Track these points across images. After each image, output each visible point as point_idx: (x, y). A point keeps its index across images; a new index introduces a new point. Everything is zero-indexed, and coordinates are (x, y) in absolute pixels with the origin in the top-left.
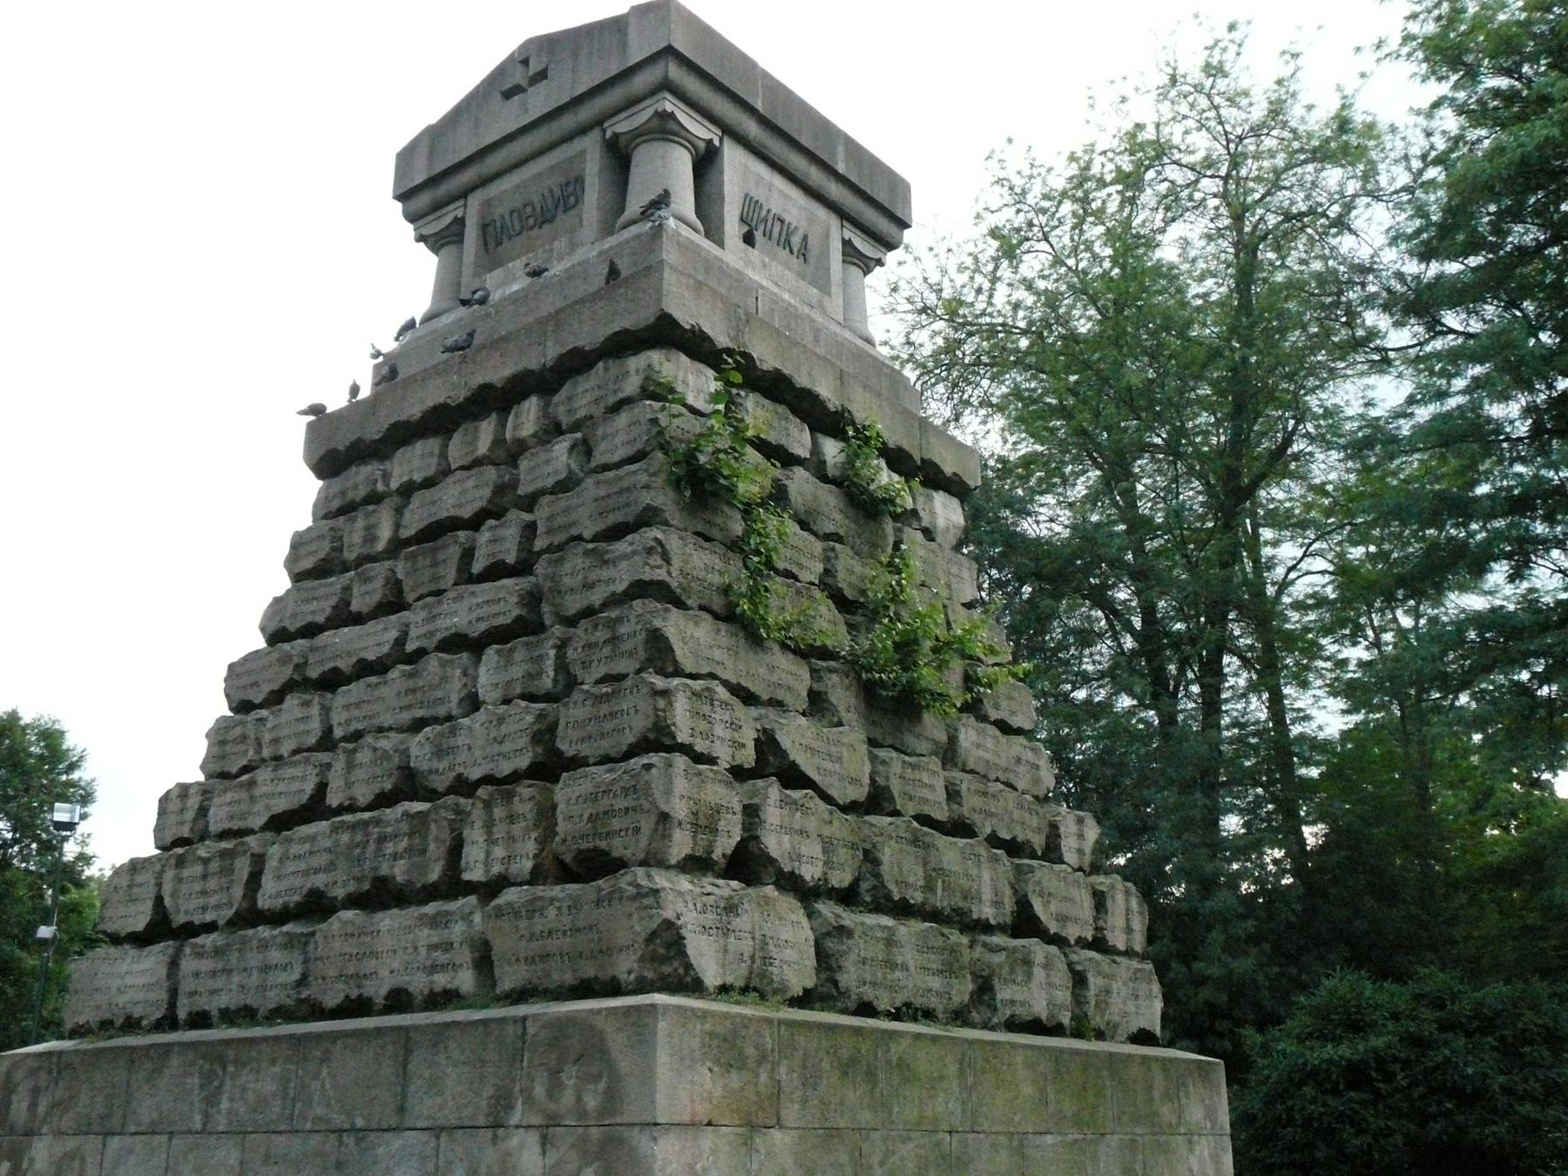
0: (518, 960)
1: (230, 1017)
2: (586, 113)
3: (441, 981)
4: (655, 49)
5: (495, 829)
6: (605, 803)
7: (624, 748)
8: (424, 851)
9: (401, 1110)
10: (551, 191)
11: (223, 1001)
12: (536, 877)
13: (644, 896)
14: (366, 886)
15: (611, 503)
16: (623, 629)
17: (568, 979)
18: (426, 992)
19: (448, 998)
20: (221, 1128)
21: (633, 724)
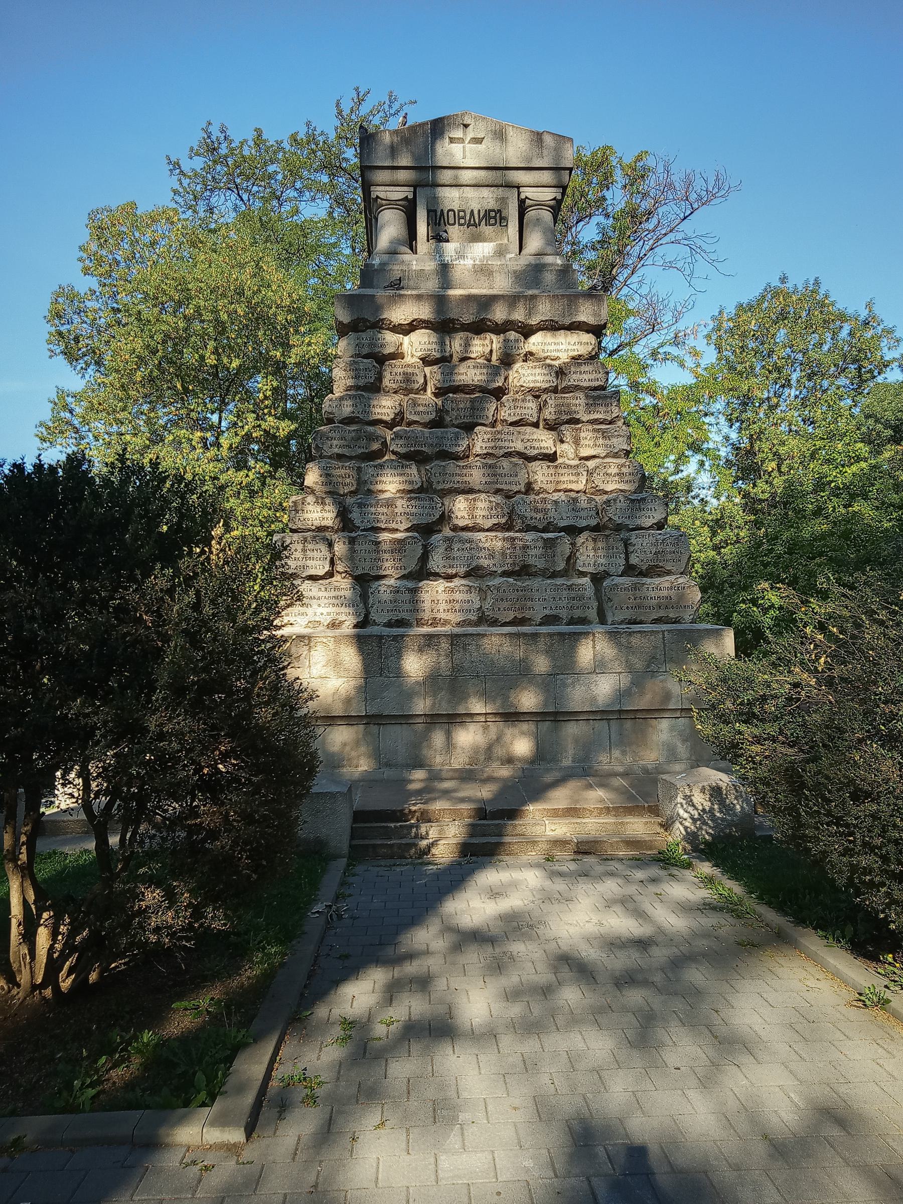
3: (577, 613)
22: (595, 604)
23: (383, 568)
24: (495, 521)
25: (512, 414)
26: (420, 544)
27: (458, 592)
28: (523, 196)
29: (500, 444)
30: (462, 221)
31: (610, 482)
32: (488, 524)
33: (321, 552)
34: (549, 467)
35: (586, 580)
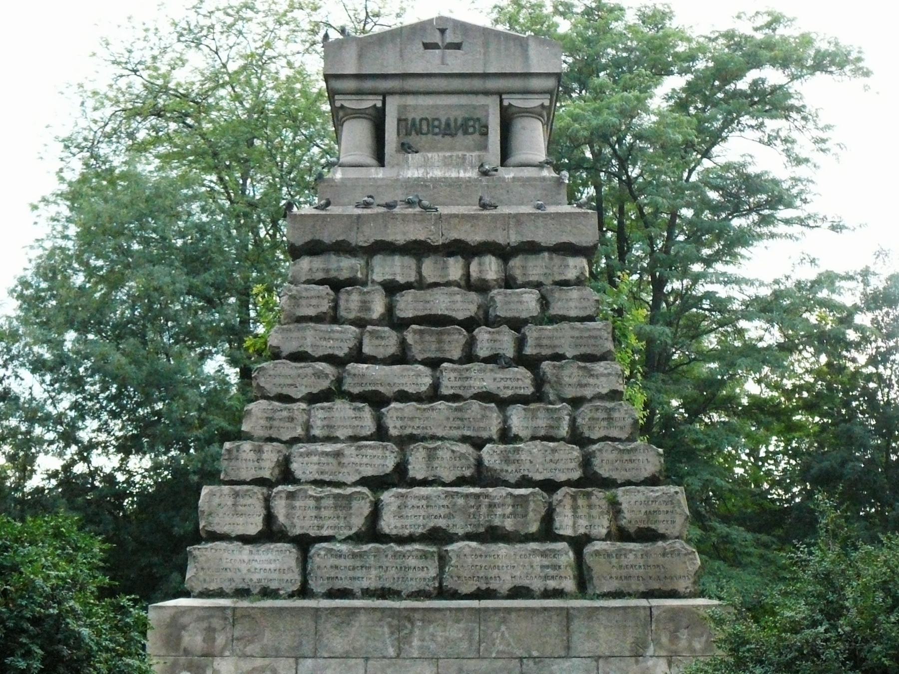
0: (611, 577)
1: (367, 593)
2: (492, 84)
3: (552, 584)
4: (551, 71)
5: (579, 511)
6: (654, 507)
7: (642, 479)
8: (525, 516)
9: (568, 648)
10: (456, 120)
11: (365, 584)
12: (608, 537)
13: (690, 554)
14: (482, 530)
15: (583, 341)
16: (616, 415)
17: (642, 588)
18: (542, 589)
19: (558, 593)
20: (415, 656)
21: (647, 468)
24: (459, 473)
26: (368, 500)
28: (506, 103)
29: (466, 384)
32: (448, 475)
35: (562, 545)
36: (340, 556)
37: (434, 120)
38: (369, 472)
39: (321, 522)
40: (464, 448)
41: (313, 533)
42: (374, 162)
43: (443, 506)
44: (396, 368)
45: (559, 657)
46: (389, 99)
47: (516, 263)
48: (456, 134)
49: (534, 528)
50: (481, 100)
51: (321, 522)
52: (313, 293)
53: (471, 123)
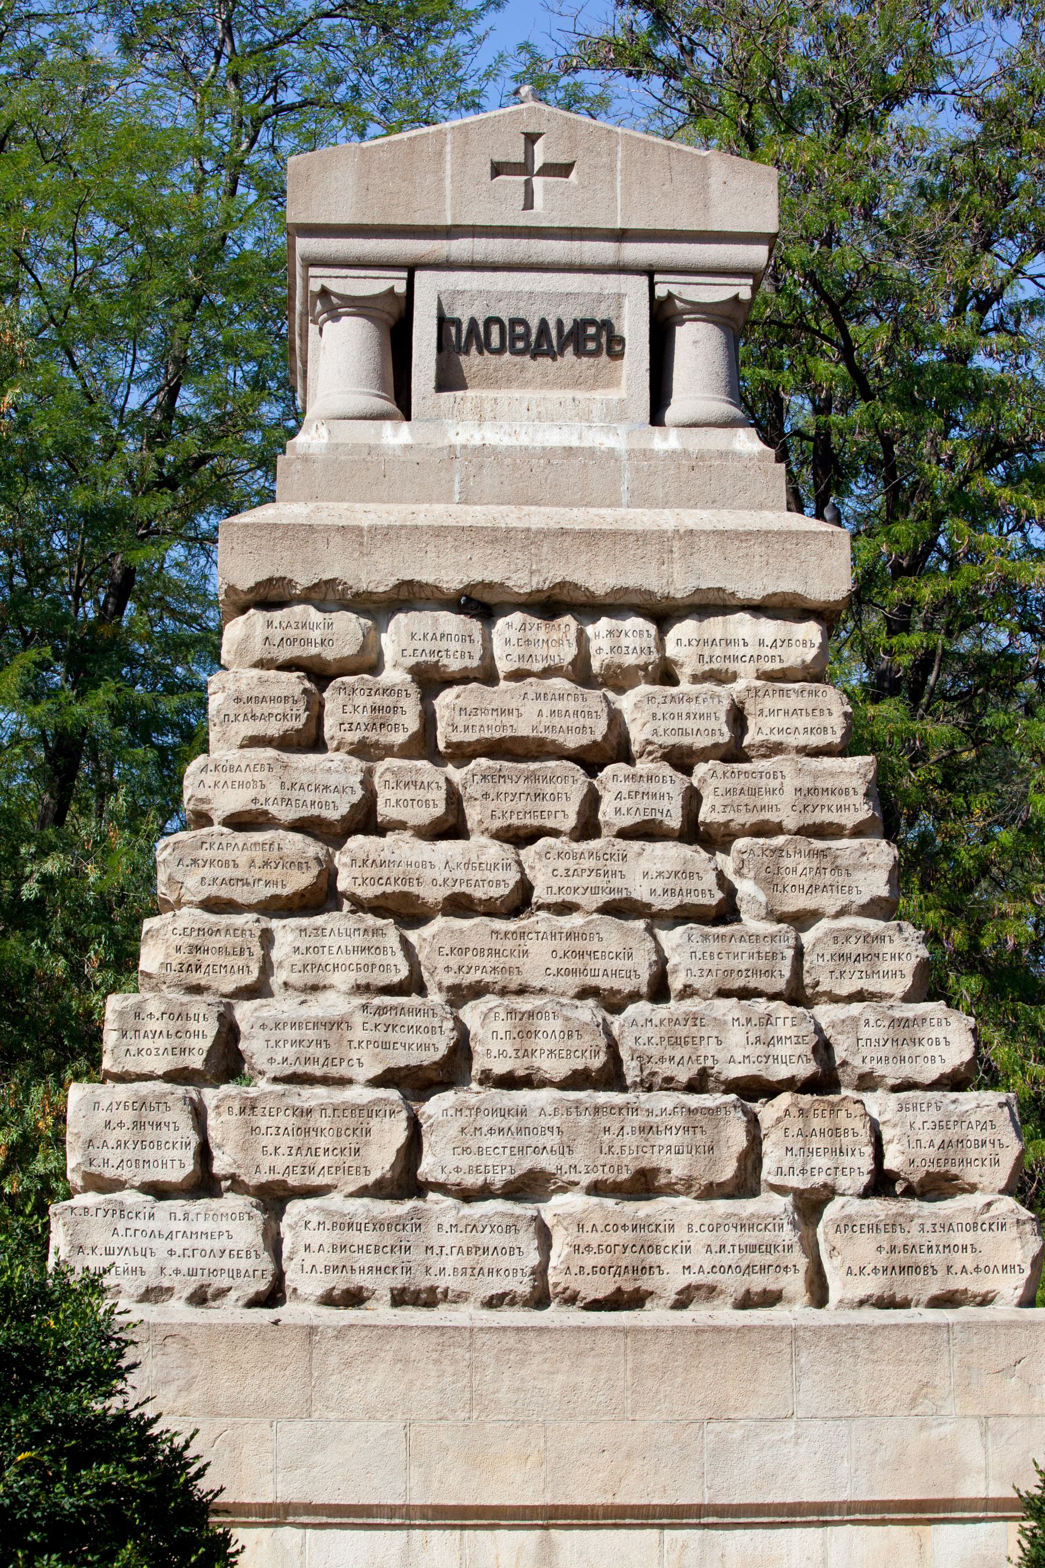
10: (560, 323)
22: (802, 1262)
23: (317, 1170)
25: (624, 811)
27: (488, 1229)
28: (661, 291)
30: (520, 345)
31: (847, 975)
32: (558, 1068)
33: (176, 1129)
34: (705, 937)
36: (350, 1226)
37: (514, 322)
38: (401, 1059)
39: (310, 1160)
40: (588, 1011)
41: (293, 1180)
42: (390, 406)
43: (551, 1129)
44: (443, 845)
45: (777, 1419)
46: (421, 277)
47: (684, 630)
48: (561, 353)
49: (727, 1171)
50: (612, 283)
51: (310, 1160)
52: (276, 691)
53: (591, 330)
